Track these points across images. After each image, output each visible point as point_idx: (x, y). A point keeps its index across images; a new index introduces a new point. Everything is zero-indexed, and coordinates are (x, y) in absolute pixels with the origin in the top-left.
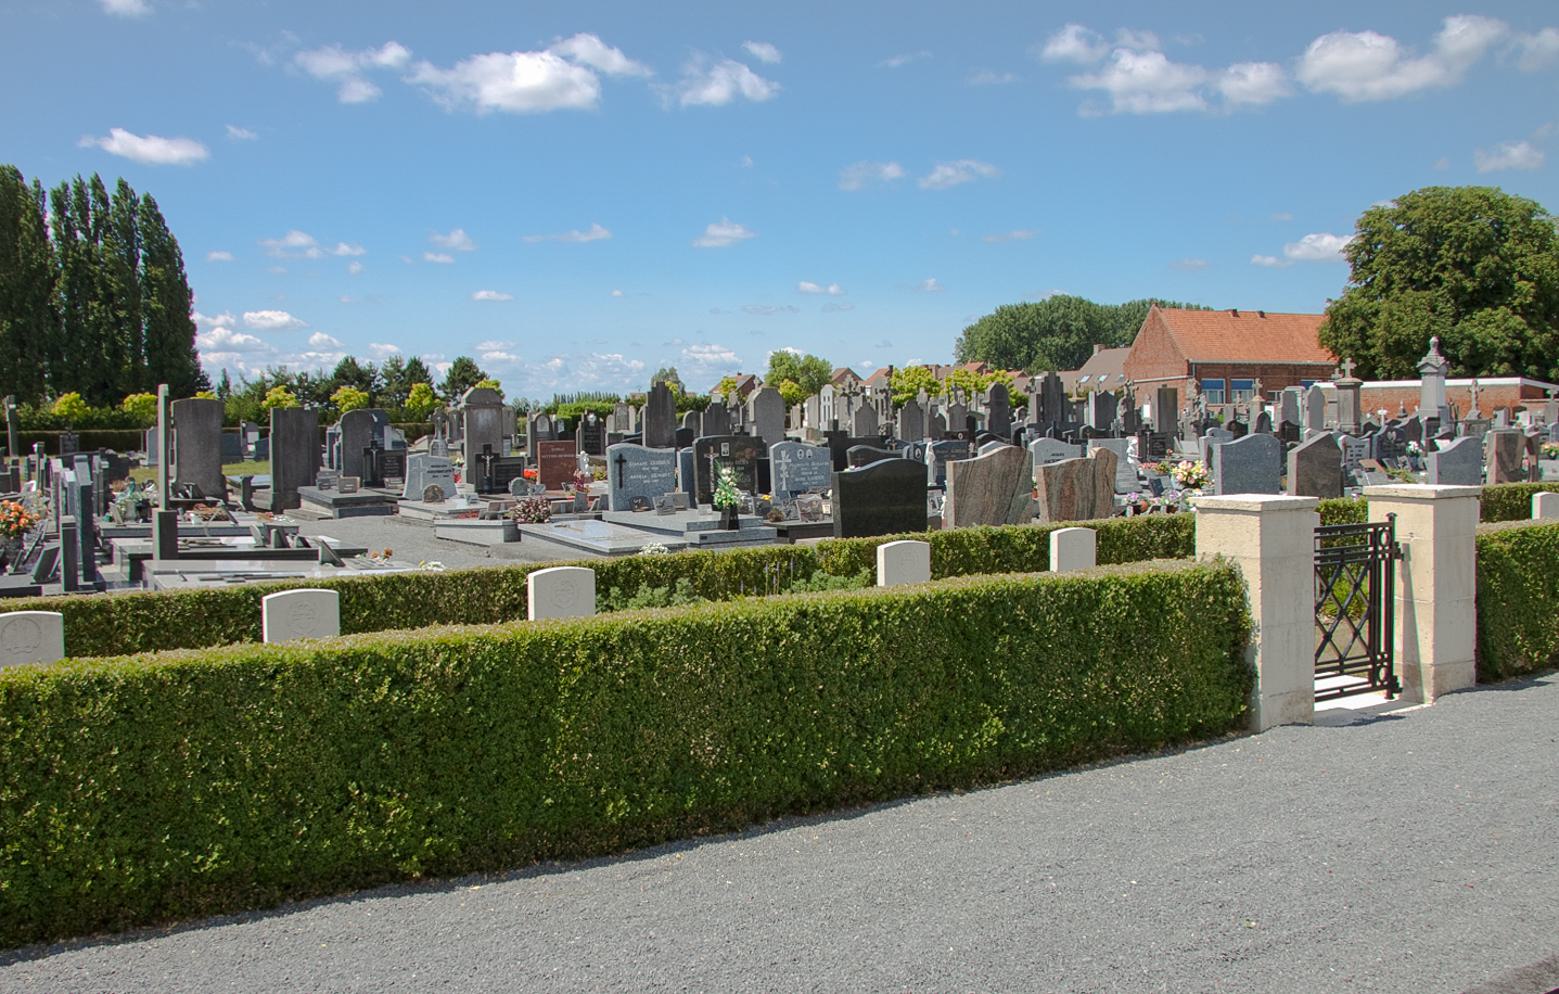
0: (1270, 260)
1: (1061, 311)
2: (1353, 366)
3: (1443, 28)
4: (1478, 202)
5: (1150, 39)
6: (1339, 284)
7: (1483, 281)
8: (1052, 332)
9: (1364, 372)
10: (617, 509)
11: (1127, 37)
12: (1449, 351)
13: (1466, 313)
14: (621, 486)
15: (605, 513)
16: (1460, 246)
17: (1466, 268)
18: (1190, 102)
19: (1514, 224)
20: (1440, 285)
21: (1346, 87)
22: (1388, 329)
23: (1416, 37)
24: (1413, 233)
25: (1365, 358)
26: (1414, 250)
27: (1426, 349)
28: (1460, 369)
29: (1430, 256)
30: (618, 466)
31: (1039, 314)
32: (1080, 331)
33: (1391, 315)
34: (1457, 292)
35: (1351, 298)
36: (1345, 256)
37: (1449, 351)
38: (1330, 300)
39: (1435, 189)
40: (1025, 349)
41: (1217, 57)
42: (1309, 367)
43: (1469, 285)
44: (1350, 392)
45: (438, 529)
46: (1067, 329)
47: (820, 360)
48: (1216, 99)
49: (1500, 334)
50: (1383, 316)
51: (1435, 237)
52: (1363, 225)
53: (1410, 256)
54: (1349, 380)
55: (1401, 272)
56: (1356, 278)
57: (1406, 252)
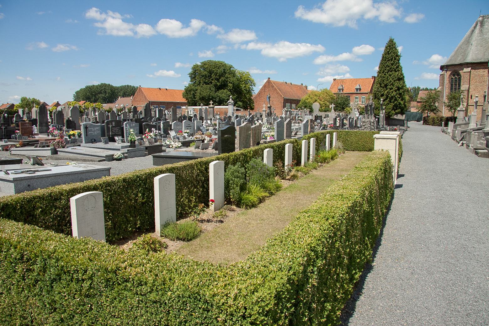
0: (151, 76)
1: (104, 87)
2: (213, 102)
3: (191, 22)
4: (220, 65)
5: (118, 15)
6: (187, 82)
7: (221, 83)
8: (101, 93)
9: (194, 104)
10: (86, 143)
11: (111, 13)
12: (214, 99)
13: (217, 91)
14: (87, 135)
15: (81, 144)
16: (216, 74)
17: (218, 80)
18: (130, 33)
19: (227, 70)
20: (212, 84)
21: (169, 33)
22: (200, 94)
23: (186, 24)
24: (205, 71)
25: (194, 101)
26: (206, 75)
27: (228, 100)
28: (217, 104)
29: (210, 77)
30: (85, 129)
31: (97, 88)
32: (109, 93)
33: (201, 90)
34: (216, 85)
35: (190, 86)
36: (189, 75)
37: (214, 99)
38: (185, 86)
39: (210, 60)
40: (94, 98)
41: (136, 21)
42: (178, 103)
43: (218, 84)
44: (212, 109)
45: (12, 151)
46: (105, 92)
47: (37, 99)
48: (136, 33)
49: (225, 96)
50: (199, 91)
51: (211, 72)
52: (193, 68)
53: (205, 76)
54: (211, 106)
55: (203, 80)
56: (191, 81)
57: (204, 75)
